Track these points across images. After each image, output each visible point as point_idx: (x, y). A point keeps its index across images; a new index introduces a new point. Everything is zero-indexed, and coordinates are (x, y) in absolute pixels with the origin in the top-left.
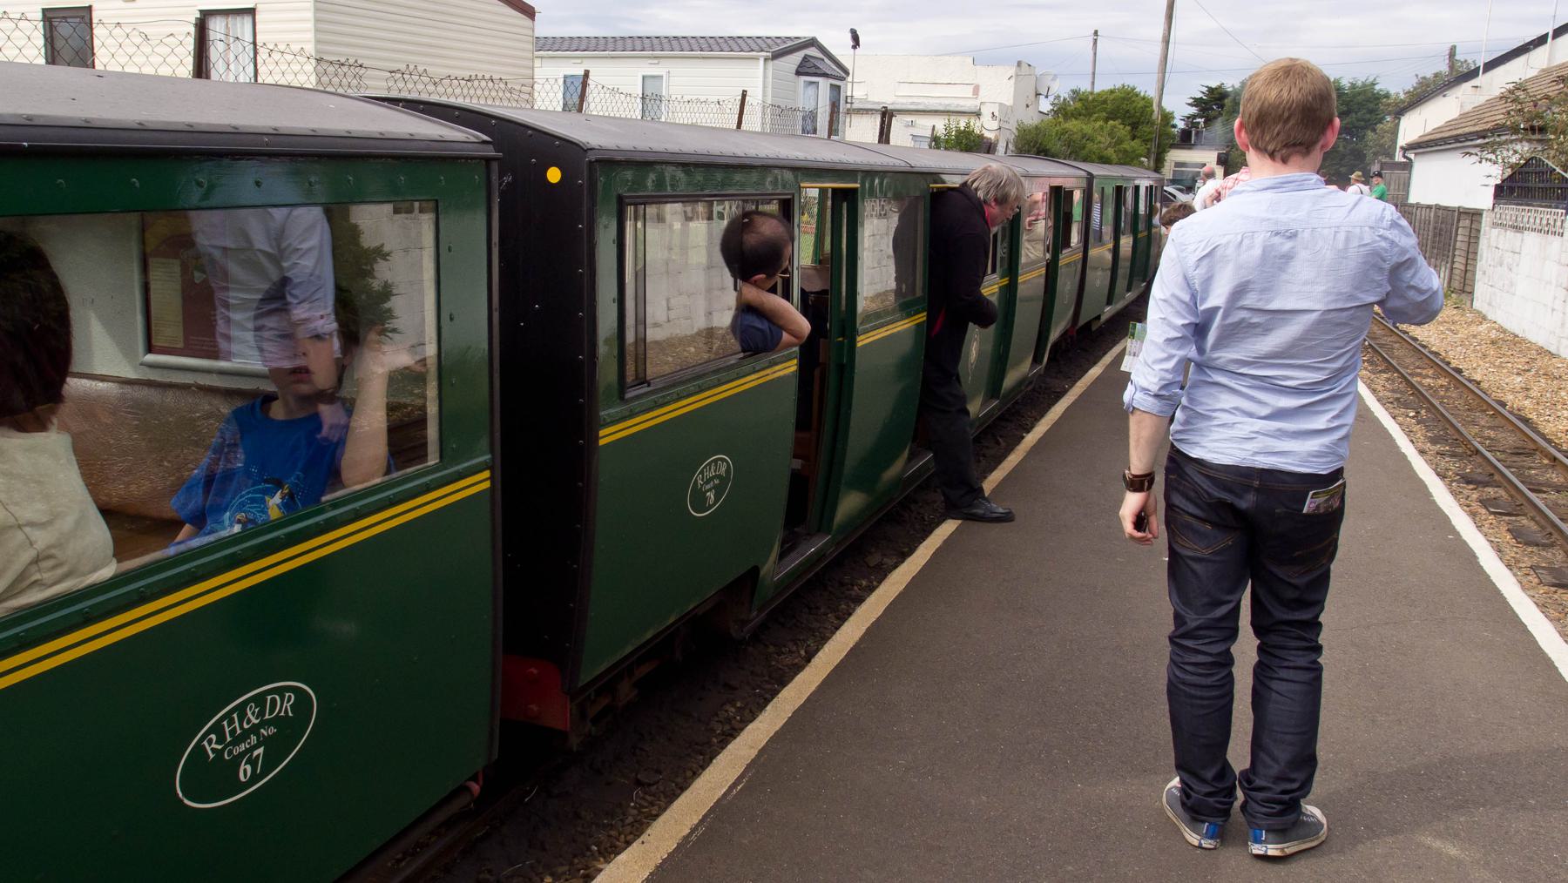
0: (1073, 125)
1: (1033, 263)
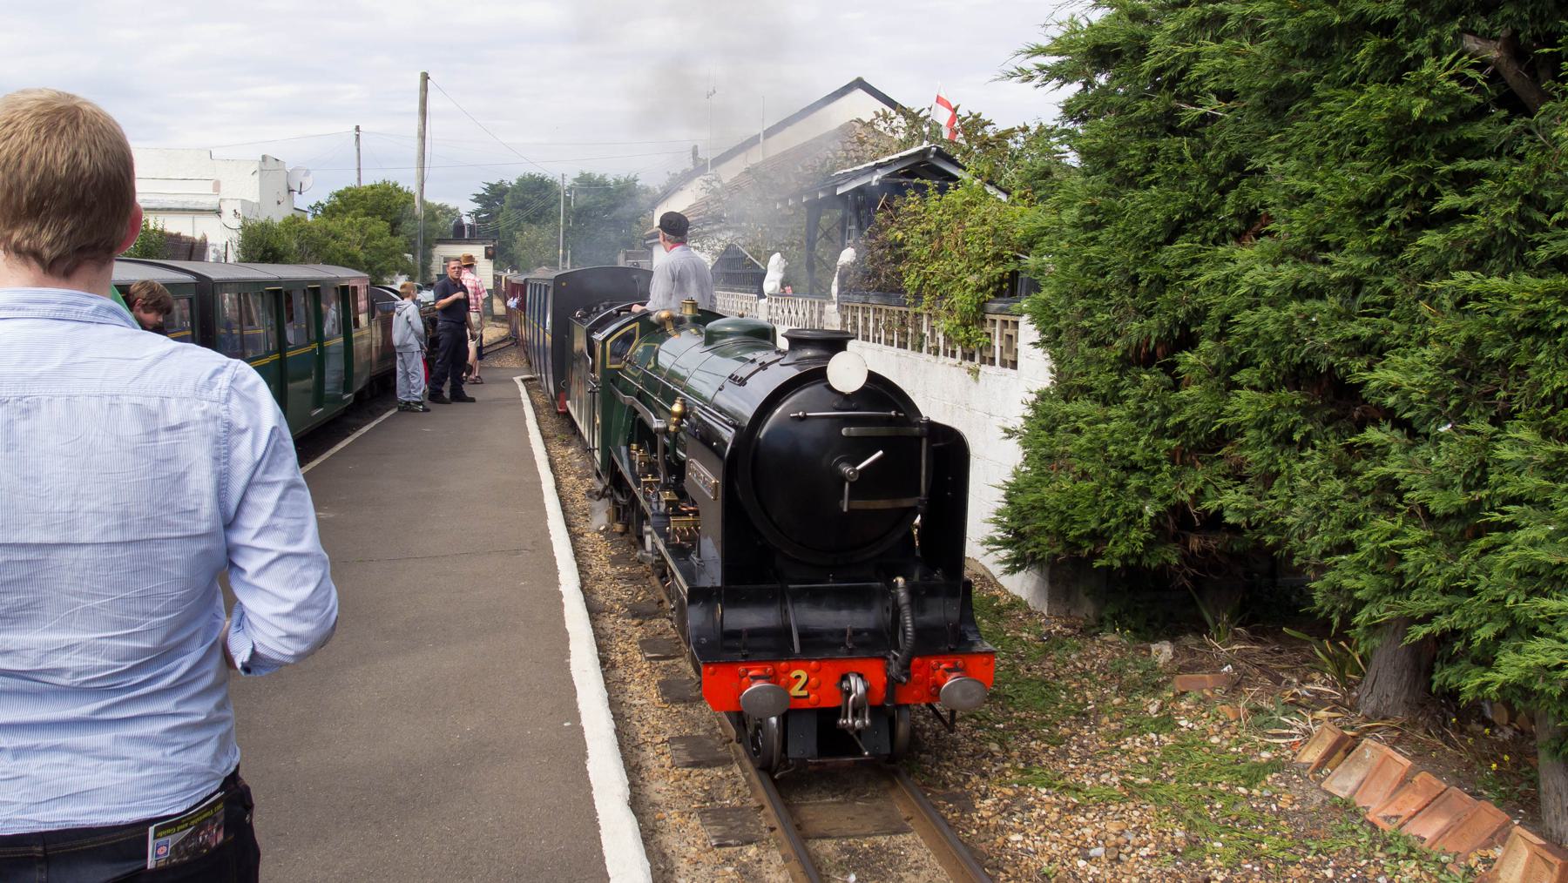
0: (334, 225)
1: (713, 298)
